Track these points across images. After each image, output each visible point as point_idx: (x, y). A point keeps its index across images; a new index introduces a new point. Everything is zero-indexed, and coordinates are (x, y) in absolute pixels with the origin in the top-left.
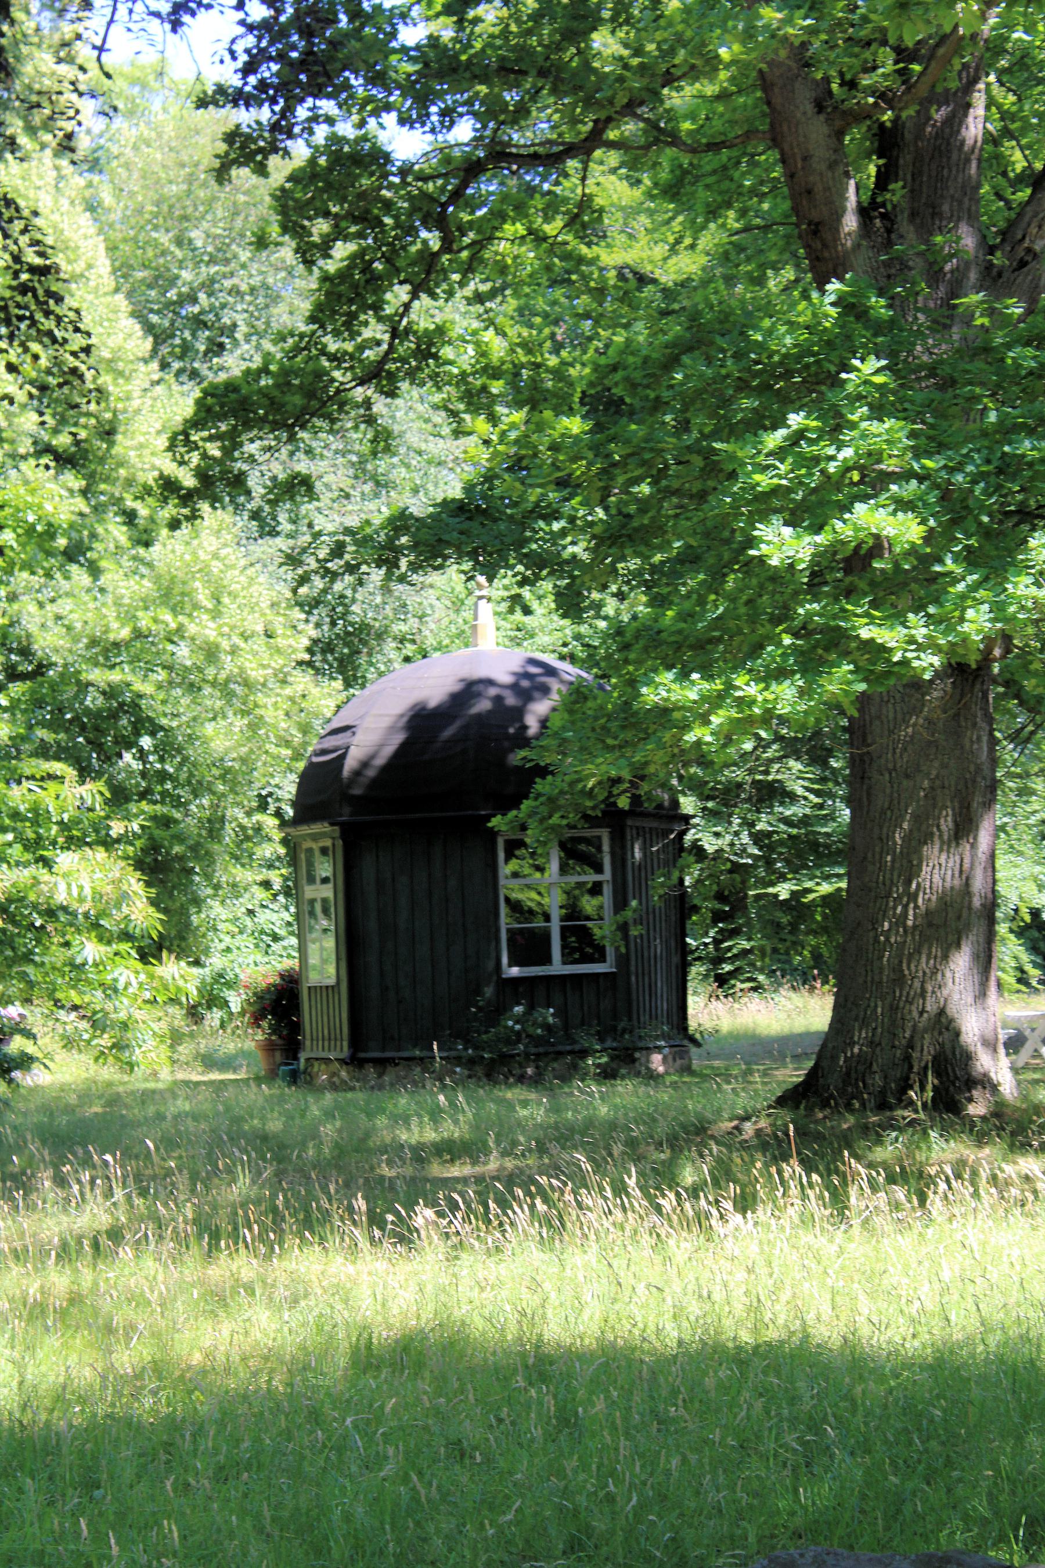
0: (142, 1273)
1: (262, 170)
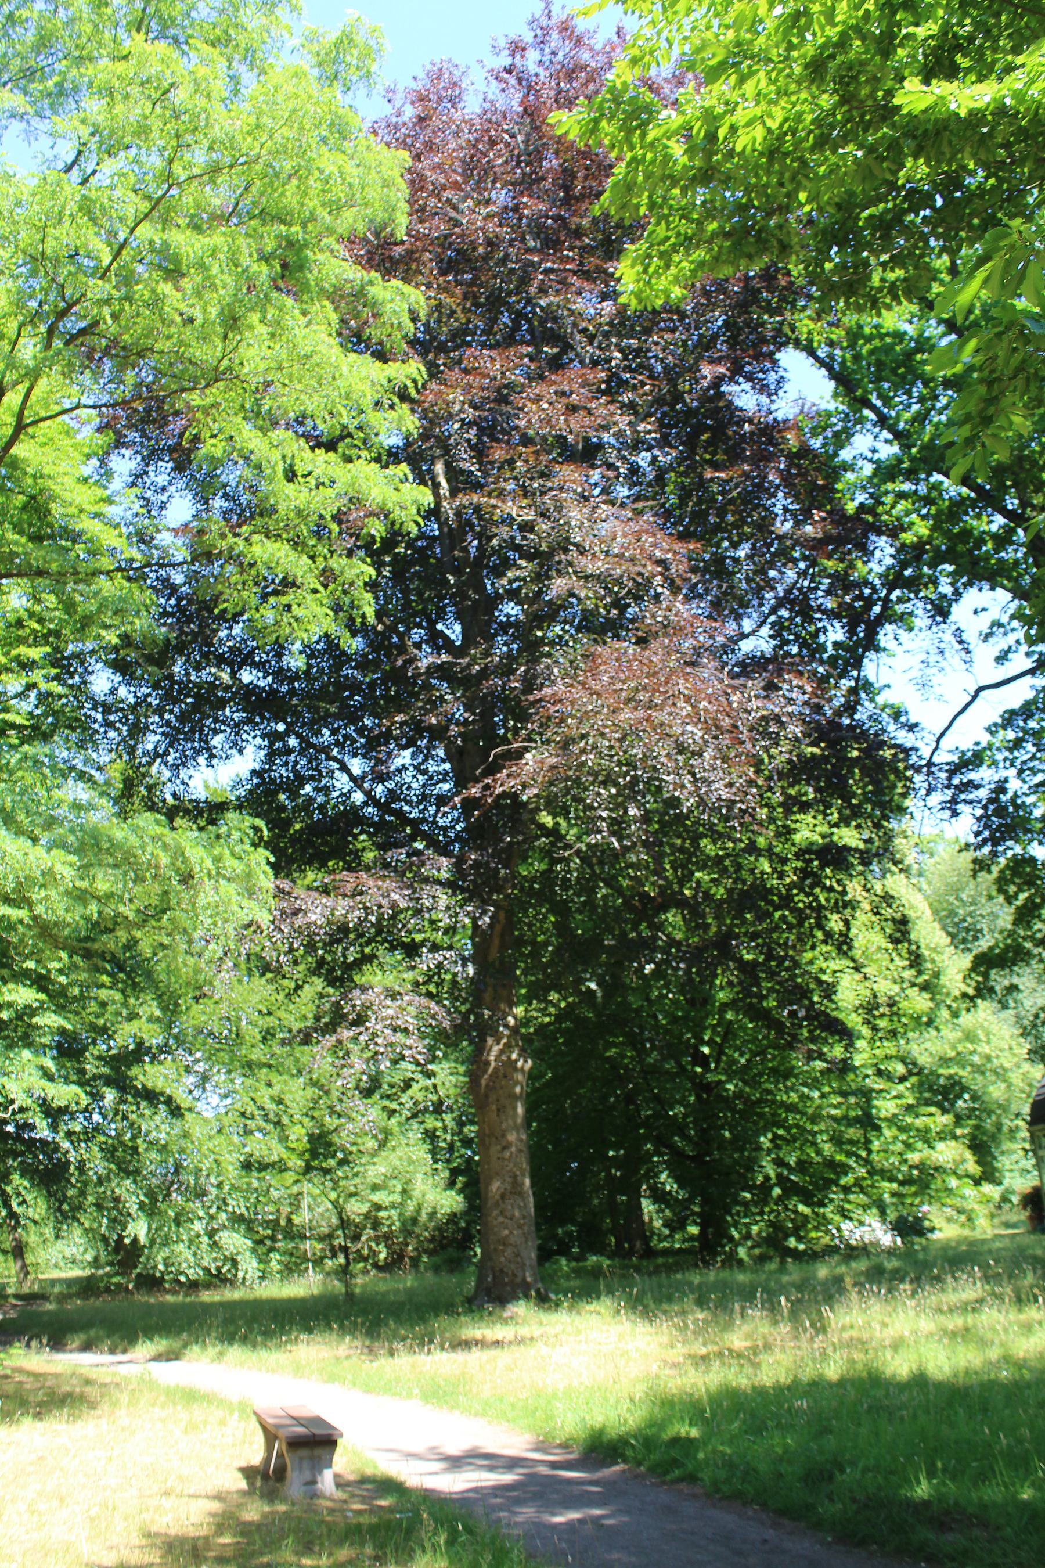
0: (991, 1317)
1: (989, 872)
